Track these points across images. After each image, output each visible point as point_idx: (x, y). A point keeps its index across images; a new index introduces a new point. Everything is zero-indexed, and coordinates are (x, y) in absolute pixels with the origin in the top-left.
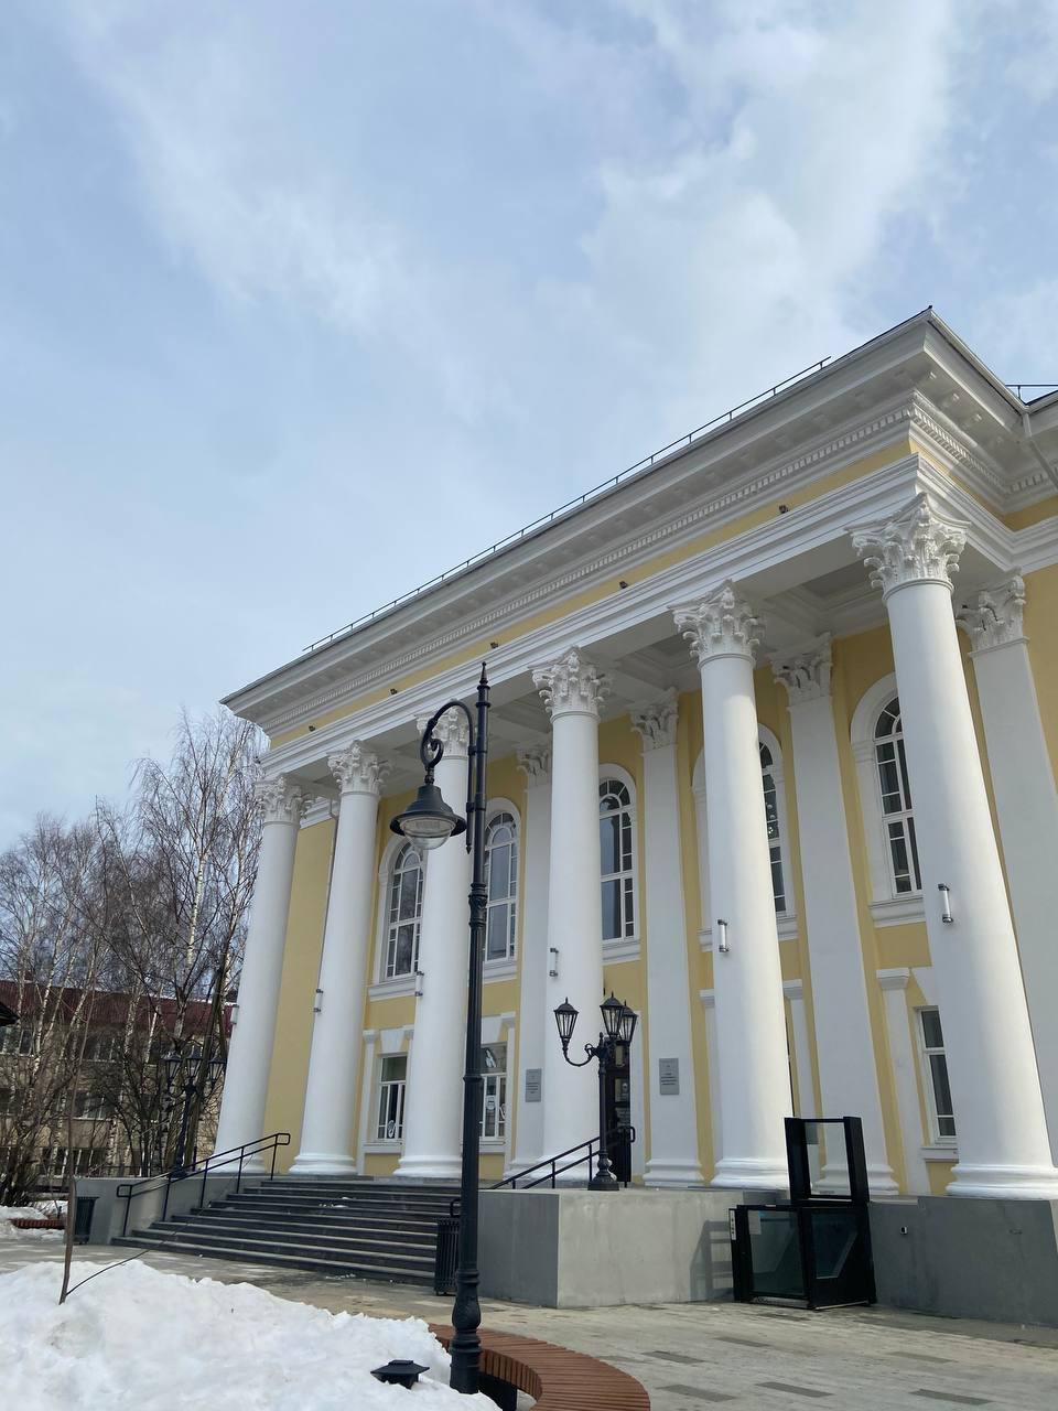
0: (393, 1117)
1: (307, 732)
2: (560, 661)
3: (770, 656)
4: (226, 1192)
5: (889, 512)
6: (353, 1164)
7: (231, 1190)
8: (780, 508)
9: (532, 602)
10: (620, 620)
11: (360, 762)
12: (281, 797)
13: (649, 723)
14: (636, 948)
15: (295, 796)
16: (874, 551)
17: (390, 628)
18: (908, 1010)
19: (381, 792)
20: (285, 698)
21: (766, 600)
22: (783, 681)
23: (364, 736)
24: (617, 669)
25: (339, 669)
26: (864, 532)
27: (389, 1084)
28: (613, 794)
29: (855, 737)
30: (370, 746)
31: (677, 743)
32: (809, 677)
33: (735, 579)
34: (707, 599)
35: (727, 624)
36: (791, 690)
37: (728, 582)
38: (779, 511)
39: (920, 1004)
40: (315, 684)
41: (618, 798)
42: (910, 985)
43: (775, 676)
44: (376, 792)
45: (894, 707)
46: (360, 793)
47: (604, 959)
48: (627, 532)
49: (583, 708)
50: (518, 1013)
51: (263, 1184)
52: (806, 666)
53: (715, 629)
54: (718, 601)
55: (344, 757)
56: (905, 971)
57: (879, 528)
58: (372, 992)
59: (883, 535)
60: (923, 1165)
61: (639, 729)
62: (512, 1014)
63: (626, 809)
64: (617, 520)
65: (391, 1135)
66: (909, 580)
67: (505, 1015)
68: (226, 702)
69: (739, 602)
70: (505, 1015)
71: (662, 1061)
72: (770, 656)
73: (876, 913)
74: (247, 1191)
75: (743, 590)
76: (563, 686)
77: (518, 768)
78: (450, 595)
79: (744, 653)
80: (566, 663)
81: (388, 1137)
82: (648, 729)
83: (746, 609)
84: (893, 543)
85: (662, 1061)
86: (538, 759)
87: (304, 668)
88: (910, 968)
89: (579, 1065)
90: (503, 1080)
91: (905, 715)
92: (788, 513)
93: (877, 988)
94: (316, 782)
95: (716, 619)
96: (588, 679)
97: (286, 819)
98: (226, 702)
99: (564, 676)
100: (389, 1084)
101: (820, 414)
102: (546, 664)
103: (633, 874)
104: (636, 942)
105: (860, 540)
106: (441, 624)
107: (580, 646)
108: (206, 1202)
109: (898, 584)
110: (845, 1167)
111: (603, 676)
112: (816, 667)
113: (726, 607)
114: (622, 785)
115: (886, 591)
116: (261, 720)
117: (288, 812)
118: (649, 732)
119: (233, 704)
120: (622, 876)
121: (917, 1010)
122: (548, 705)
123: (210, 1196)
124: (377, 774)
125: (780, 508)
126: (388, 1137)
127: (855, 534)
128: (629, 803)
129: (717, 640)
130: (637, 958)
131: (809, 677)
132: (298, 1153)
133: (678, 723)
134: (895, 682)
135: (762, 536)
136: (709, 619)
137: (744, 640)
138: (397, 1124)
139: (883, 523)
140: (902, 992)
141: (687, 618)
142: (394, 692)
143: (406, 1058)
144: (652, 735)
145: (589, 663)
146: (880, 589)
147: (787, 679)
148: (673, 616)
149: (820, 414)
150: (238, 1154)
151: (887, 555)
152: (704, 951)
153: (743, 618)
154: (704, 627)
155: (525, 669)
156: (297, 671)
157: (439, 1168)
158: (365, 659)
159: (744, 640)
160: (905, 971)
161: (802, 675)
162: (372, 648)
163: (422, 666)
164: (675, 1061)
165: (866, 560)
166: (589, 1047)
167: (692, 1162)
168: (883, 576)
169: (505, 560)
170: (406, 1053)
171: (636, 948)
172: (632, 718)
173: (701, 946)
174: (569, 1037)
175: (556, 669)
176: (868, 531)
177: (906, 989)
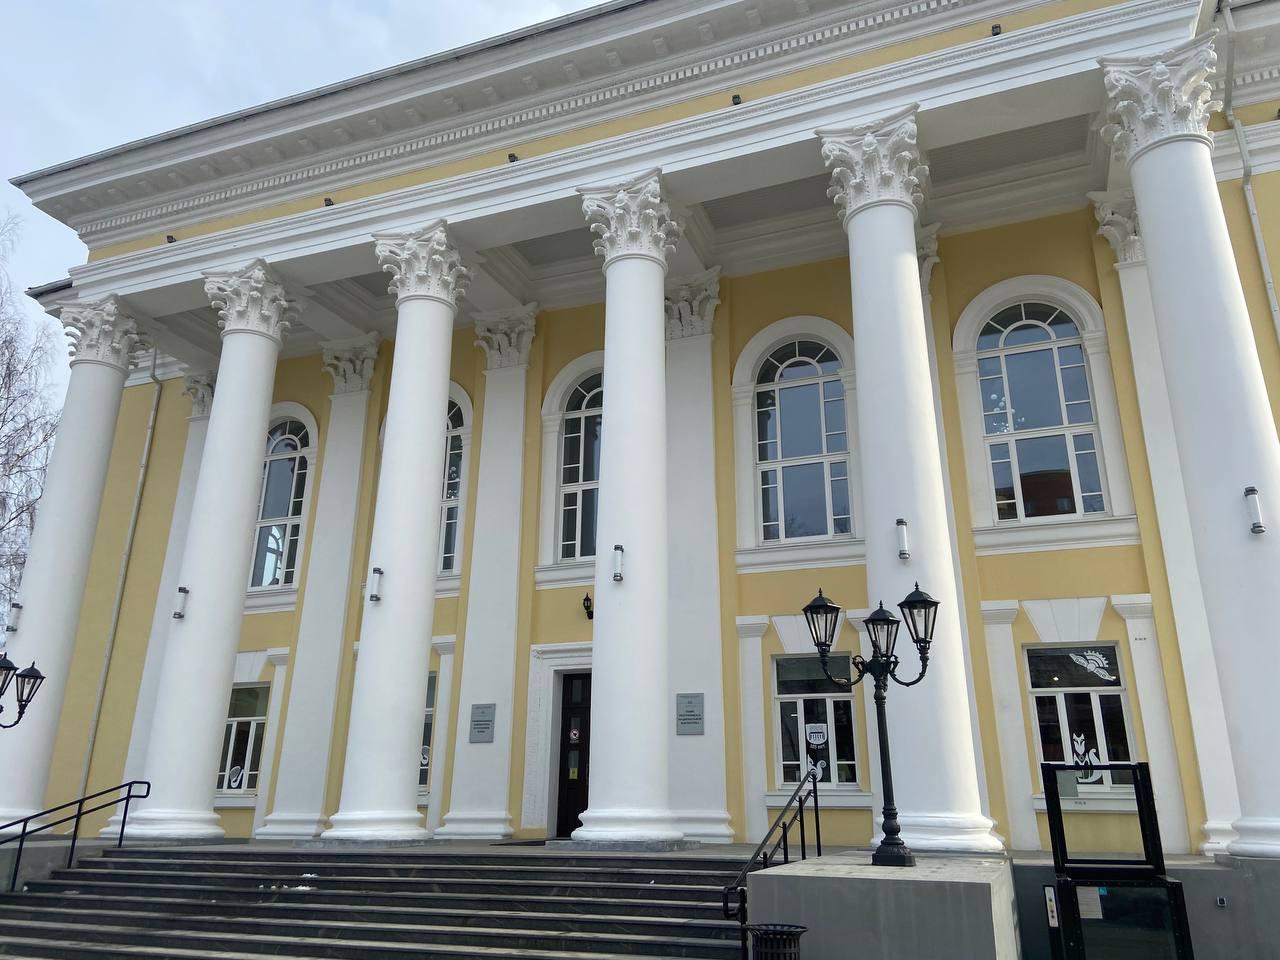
0: (239, 760)
1: (981, 36)
2: (630, 188)
3: (323, 344)
4: (50, 866)
5: (1157, 50)
6: (422, 823)
7: (57, 864)
8: (168, 237)
9: (166, 215)
10: (1046, 64)
11: (114, 324)
12: (107, 327)
13: (498, 338)
14: (456, 584)
15: (126, 333)
16: (843, 161)
17: (266, 129)
18: (1016, 647)
19: (284, 338)
20: (129, 191)
21: (477, 252)
22: (484, 344)
23: (273, 256)
24: (481, 265)
25: (303, 142)
26: (388, 242)
27: (235, 721)
28: (286, 433)
29: (958, 345)
30: (277, 274)
31: (371, 389)
32: (510, 343)
33: (269, 260)
34: (417, 236)
35: (647, 220)
36: (338, 381)
37: (443, 222)
38: (990, 33)
39: (1030, 640)
40: (190, 176)
41: (296, 439)
42: (1019, 619)
43: (476, 337)
44: (278, 336)
45: (595, 381)
46: (261, 334)
47: (437, 591)
48: (419, 125)
49: (262, 328)
50: (294, 651)
51: (106, 853)
52: (509, 332)
53: (421, 268)
54: (428, 240)
55: (234, 281)
56: (1013, 604)
57: (226, 279)
58: (540, 576)
59: (404, 249)
60: (766, 812)
61: (331, 370)
62: (285, 650)
63: (304, 452)
64: (656, 37)
65: (234, 785)
66: (1180, 133)
67: (272, 651)
68: (20, 183)
69: (450, 247)
70: (272, 651)
71: (476, 708)
72: (323, 344)
73: (980, 539)
74: (83, 864)
75: (671, 186)
76: (421, 268)
77: (323, 370)
78: (456, 75)
79: (449, 300)
80: (250, 278)
81: (230, 787)
82: (341, 370)
83: (130, 324)
84: (622, 212)
85: (476, 708)
86: (352, 361)
87: (108, 167)
88: (1020, 601)
89: (908, 685)
90: (261, 727)
91: (609, 388)
92: (334, 206)
93: (731, 637)
94: (155, 319)
95: (634, 213)
96: (274, 300)
97: (112, 360)
98: (20, 183)
99: (98, 323)
100: (235, 721)
101: (570, 62)
102: (397, 236)
103: (302, 520)
104: (456, 577)
105: (831, 147)
106: (425, 118)
107: (120, 294)
108: (19, 882)
109: (1165, 136)
110: (1134, 807)
111: (145, 334)
112: (519, 334)
113: (437, 247)
114: (303, 427)
115: (608, 259)
116: (74, 220)
117: (116, 351)
118: (342, 372)
119: (37, 186)
120: (578, 488)
121: (773, 656)
122: (222, 319)
123: (26, 873)
124: (283, 313)
125: (168, 237)
126: (230, 787)
127: (380, 242)
128: (307, 445)
129: (634, 237)
130: (292, 608)
131: (510, 343)
132: (585, 807)
133: (374, 369)
134: (272, 411)
135: (707, 126)
136: (415, 256)
137: (451, 286)
138: (246, 772)
139: (406, 237)
140: (759, 639)
141: (391, 252)
142: (329, 203)
143: (591, 674)
144: (680, 319)
145: (129, 317)
146: (395, 296)
147: (487, 342)
148: (205, 283)
149: (570, 62)
150: (73, 810)
151: (403, 266)
152: (537, 588)
153: (452, 266)
154: (621, 219)
155: (573, 193)
156: (100, 168)
157: (401, 827)
158: (286, 150)
159: (662, 244)
160: (1013, 604)
161: (504, 341)
162: (302, 134)
163: (383, 173)
164: (699, 697)
165: (837, 170)
166: (858, 660)
167: (723, 814)
168: (607, 244)
169: (549, 39)
170: (269, 683)
171: (456, 584)
172: (325, 358)
173: (536, 583)
174: (28, 701)
175: (411, 243)
176: (598, 196)
177: (763, 637)
